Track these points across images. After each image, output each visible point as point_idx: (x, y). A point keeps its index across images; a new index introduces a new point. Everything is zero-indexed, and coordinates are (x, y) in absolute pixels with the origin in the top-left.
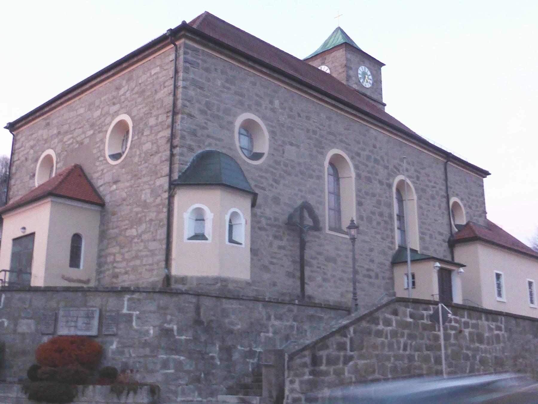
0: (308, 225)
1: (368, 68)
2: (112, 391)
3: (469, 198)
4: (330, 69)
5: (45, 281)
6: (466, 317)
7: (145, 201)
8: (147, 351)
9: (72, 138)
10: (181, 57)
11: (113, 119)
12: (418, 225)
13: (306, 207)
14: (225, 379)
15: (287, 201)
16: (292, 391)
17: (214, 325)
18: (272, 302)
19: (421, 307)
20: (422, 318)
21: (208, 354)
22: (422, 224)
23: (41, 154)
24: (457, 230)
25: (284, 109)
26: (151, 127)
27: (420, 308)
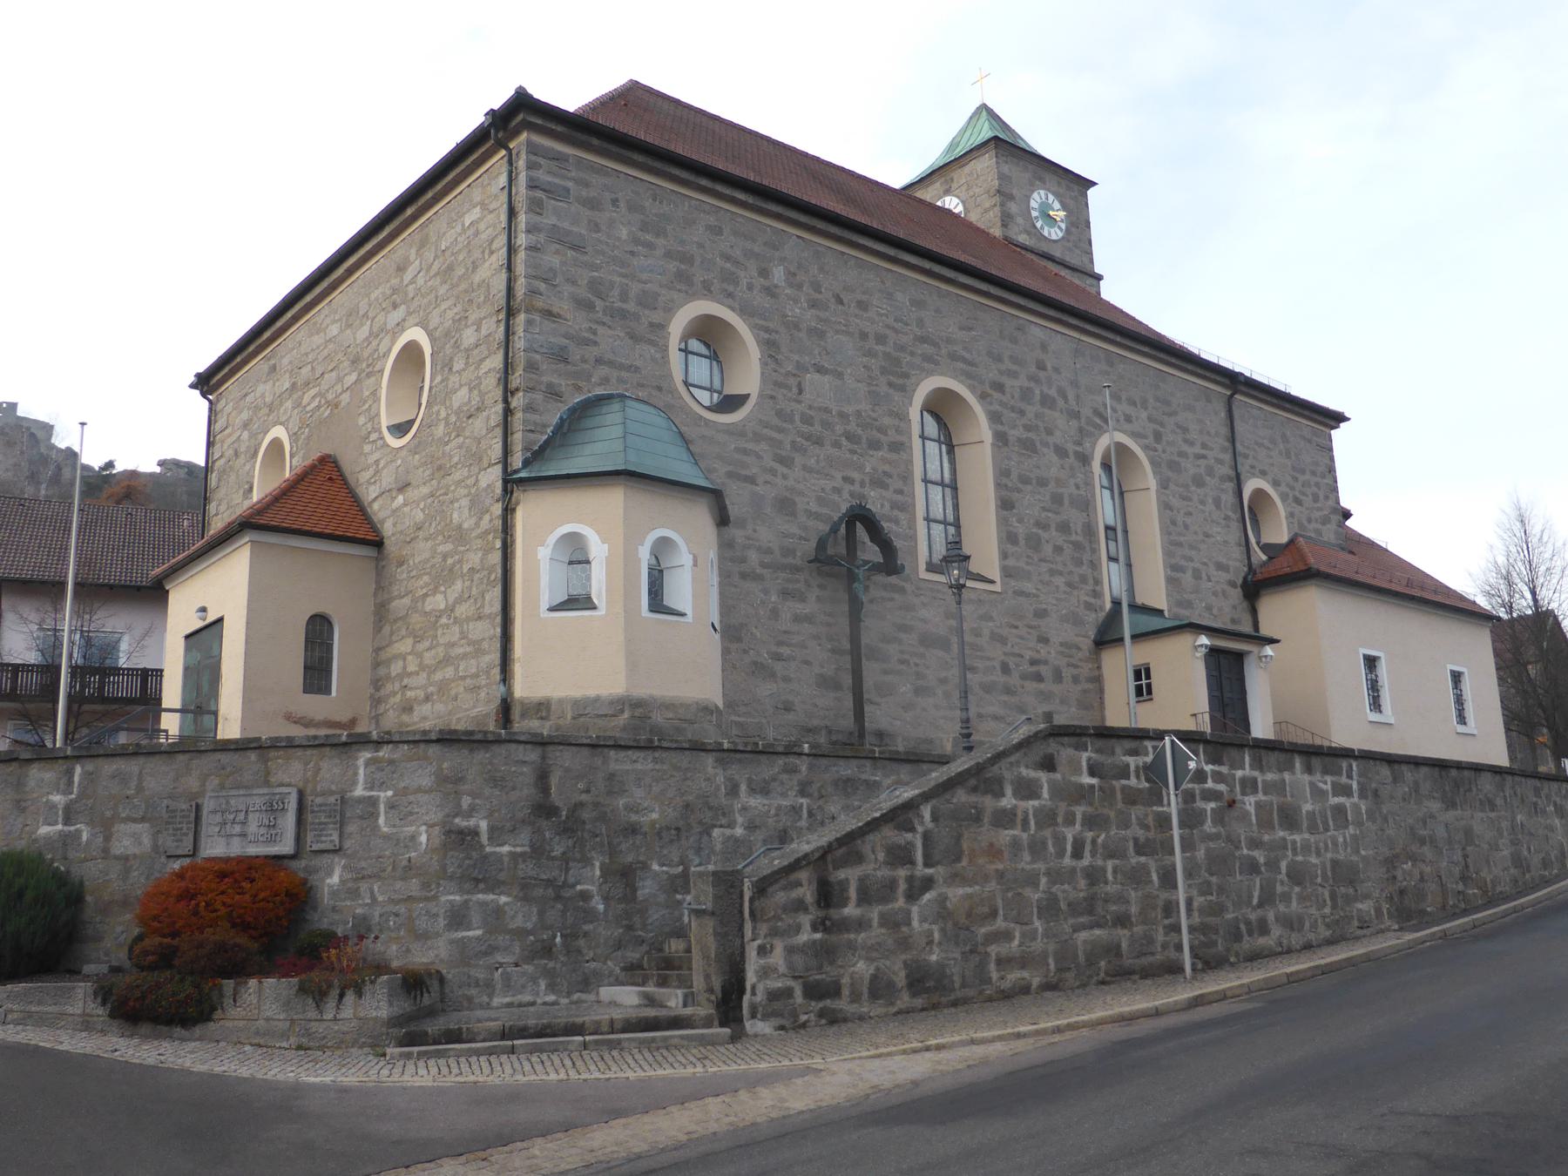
0: (866, 562)
1: (1057, 195)
2: (303, 990)
3: (1296, 479)
4: (964, 203)
5: (243, 729)
6: (1247, 766)
7: (460, 527)
8: (413, 888)
9: (319, 394)
10: (522, 178)
11: (393, 343)
12: (1163, 548)
13: (860, 517)
14: (619, 945)
15: (814, 507)
16: (765, 973)
17: (586, 815)
18: (742, 752)
19: (1120, 747)
20: (1124, 772)
21: (573, 886)
22: (1171, 546)
23: (263, 440)
24: (1264, 558)
25: (799, 287)
26: (467, 350)
27: (1118, 750)
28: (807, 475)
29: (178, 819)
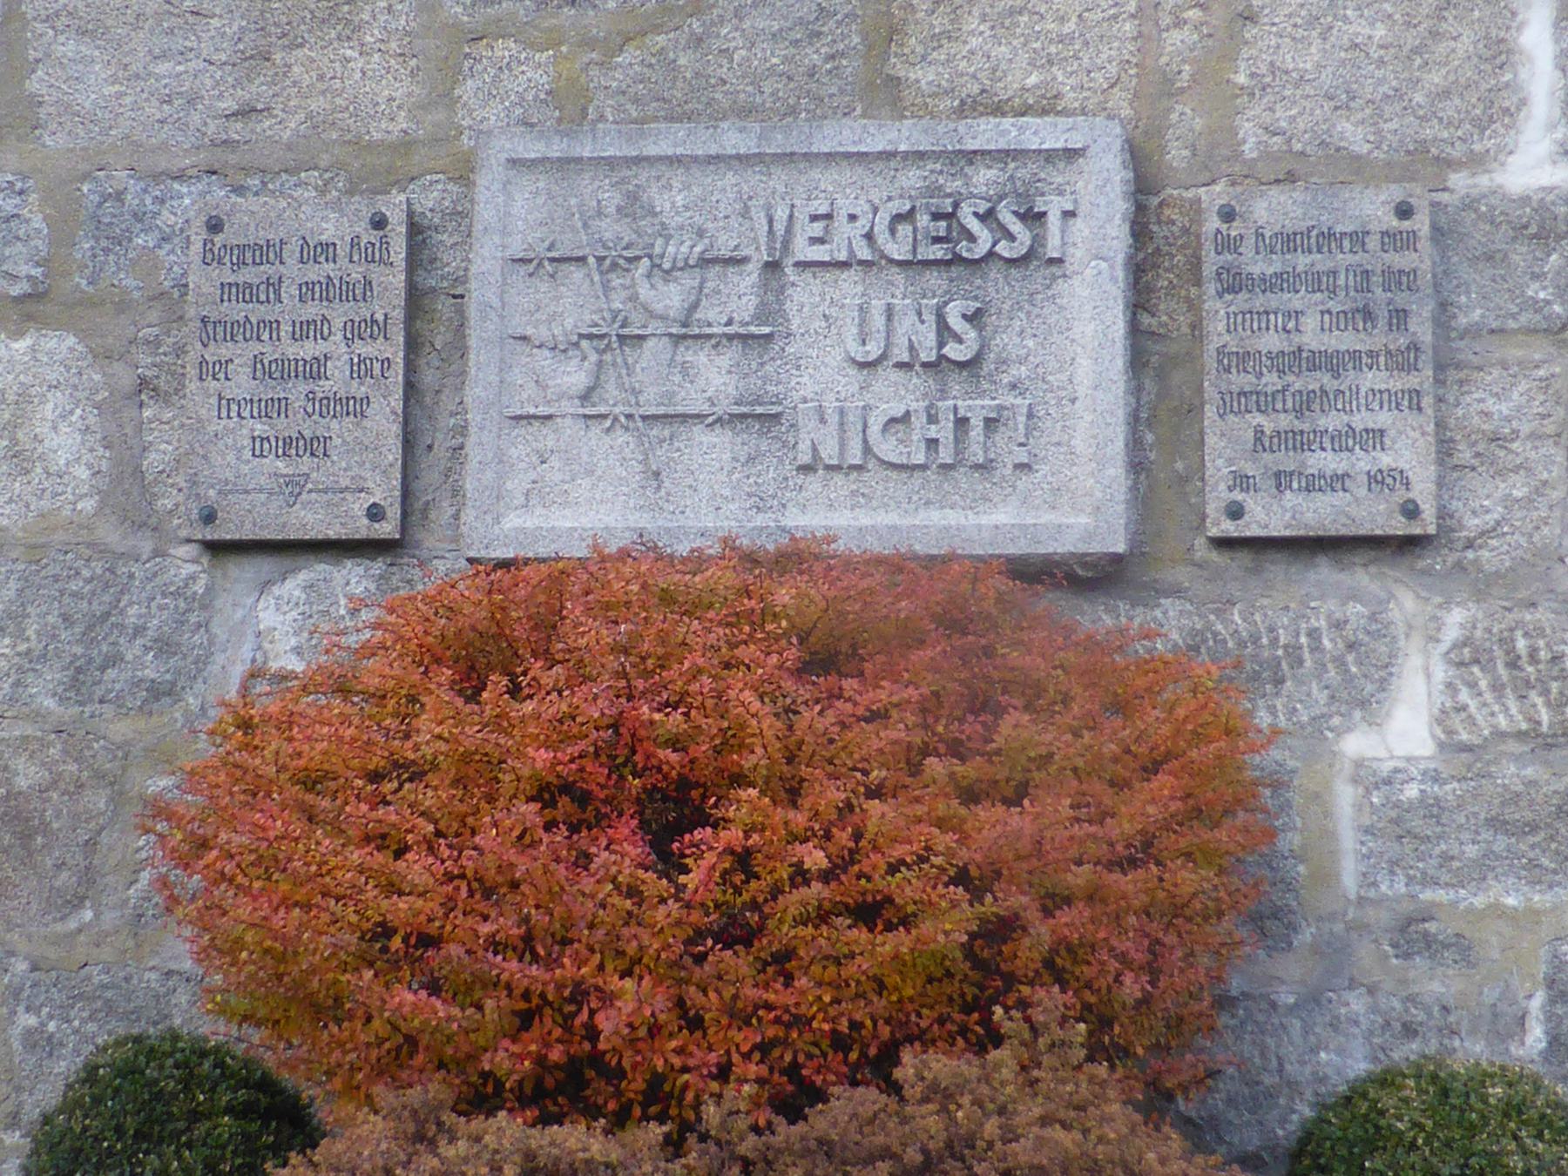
29: (290, 309)
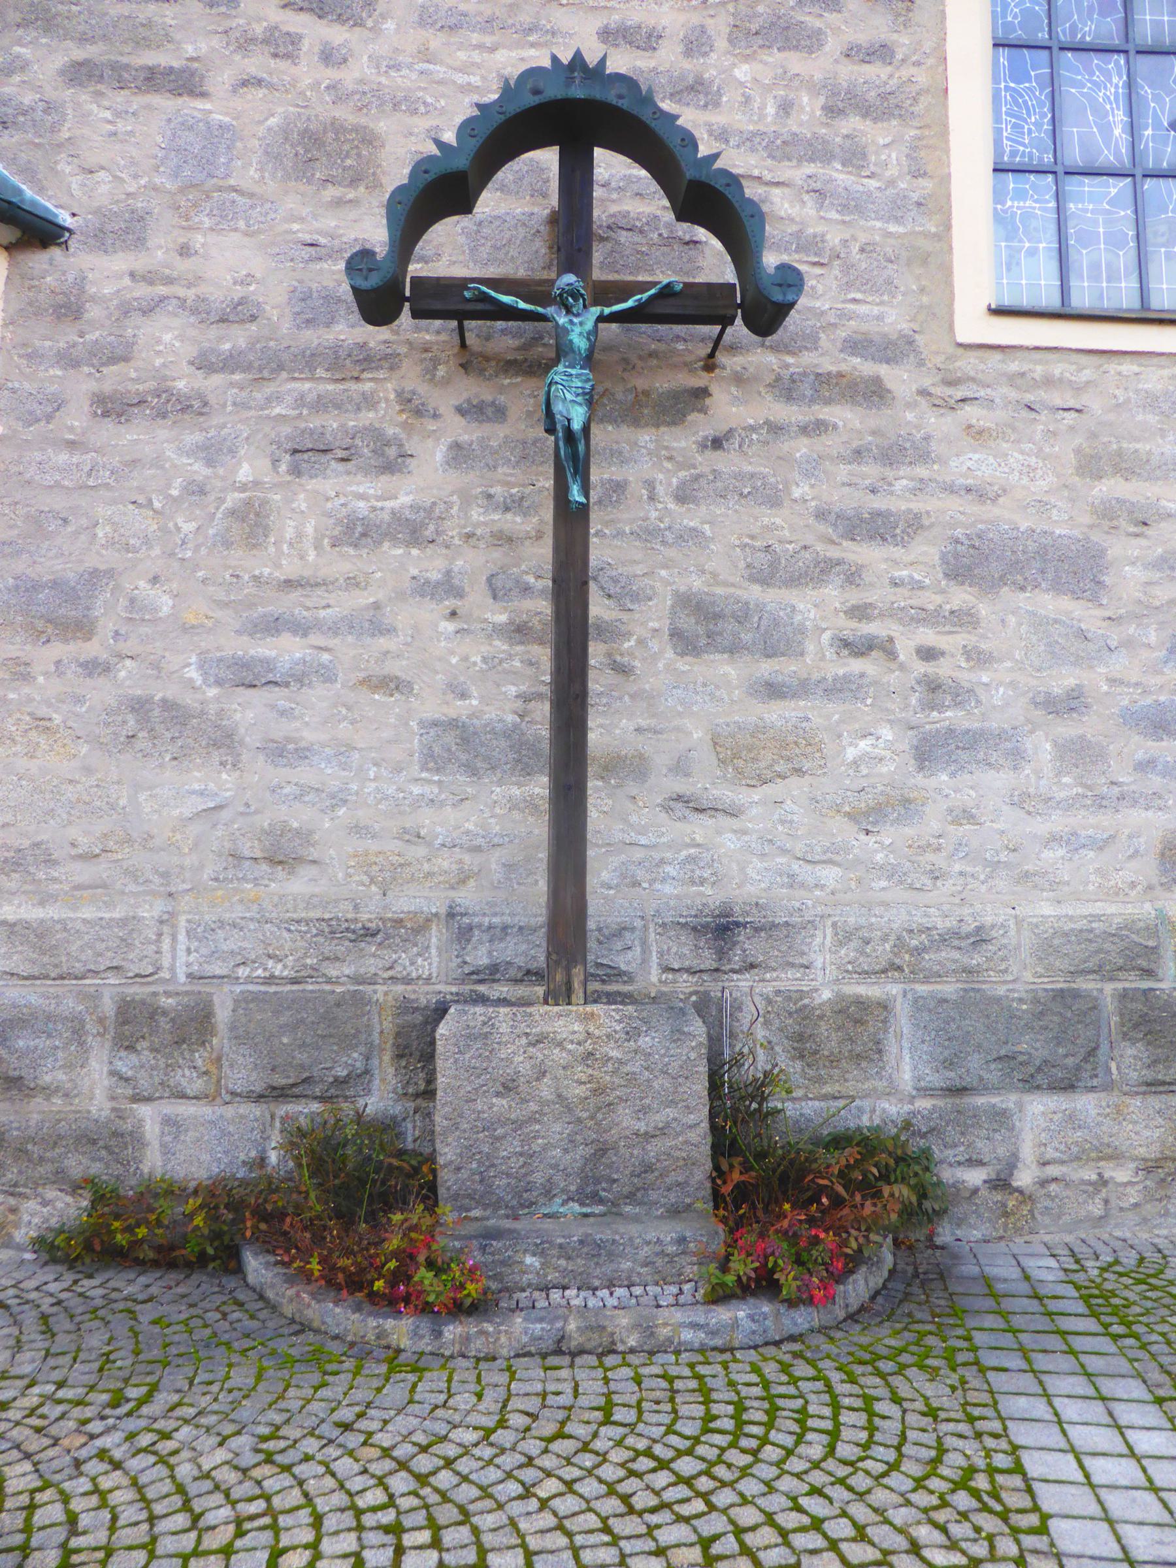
28: (436, 41)
